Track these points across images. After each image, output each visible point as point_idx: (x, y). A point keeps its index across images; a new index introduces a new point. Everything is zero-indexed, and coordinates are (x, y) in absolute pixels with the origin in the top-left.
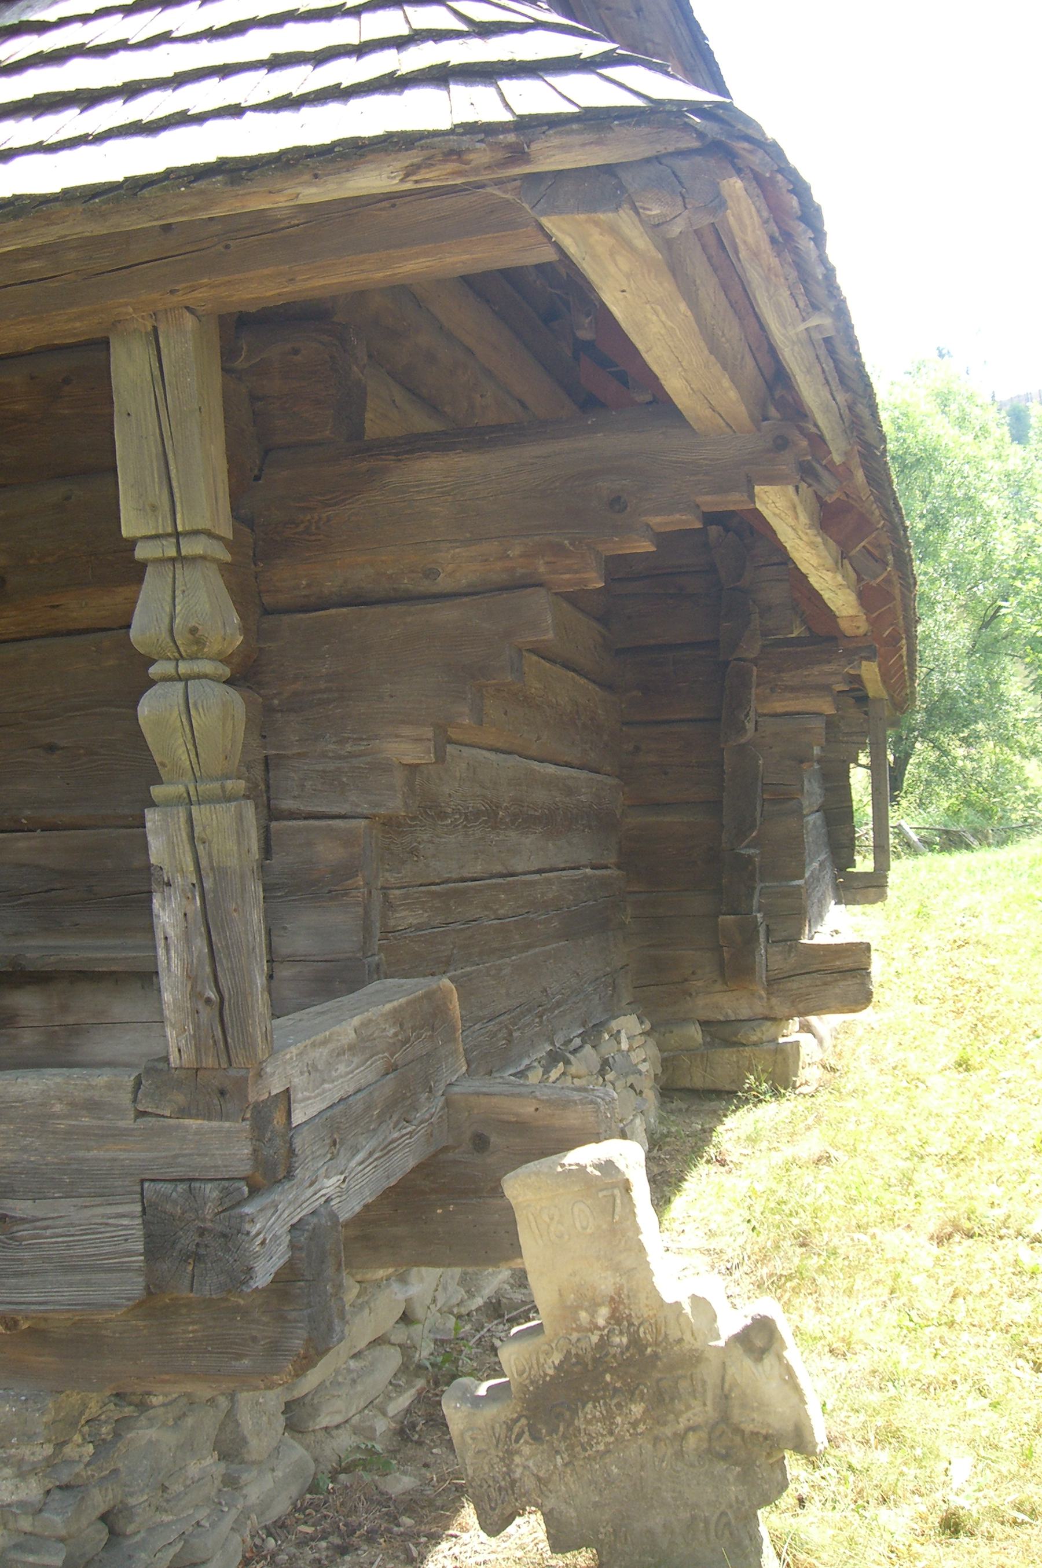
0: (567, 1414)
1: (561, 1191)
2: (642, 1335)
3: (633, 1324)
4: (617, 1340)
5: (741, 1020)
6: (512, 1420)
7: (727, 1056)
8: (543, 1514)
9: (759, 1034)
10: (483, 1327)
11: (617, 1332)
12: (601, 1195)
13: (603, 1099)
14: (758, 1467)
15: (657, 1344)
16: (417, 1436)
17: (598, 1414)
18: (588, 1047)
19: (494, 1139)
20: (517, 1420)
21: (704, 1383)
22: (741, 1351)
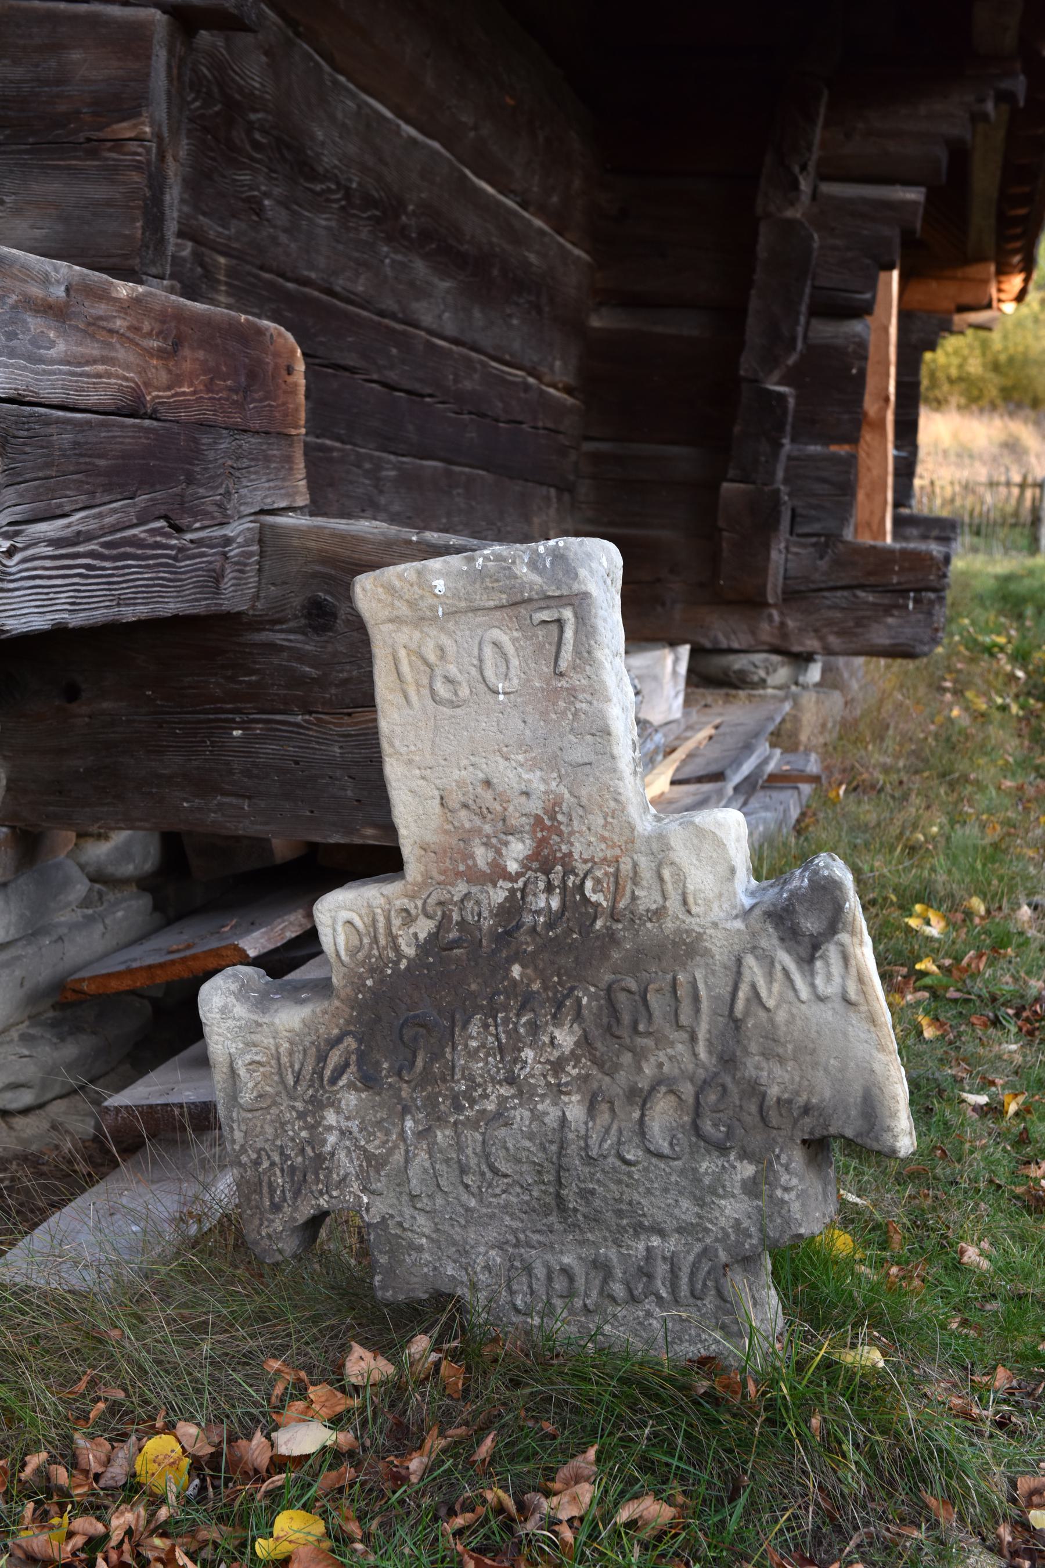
3: (573, 871)
20: (339, 1040)
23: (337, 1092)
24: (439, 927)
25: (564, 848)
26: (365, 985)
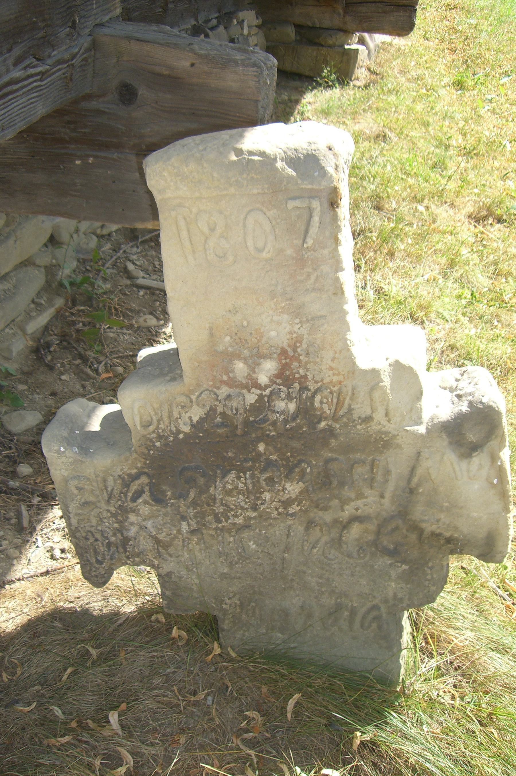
0: (201, 481)
1: (232, 190)
2: (317, 404)
3: (307, 389)
4: (280, 405)
5: (323, 29)
6: (130, 475)
7: (310, 51)
8: (159, 576)
9: (334, 40)
10: (120, 249)
11: (283, 395)
12: (291, 205)
13: (265, 64)
14: (431, 568)
15: (335, 418)
16: (49, 358)
17: (241, 485)
18: (221, 28)
19: (142, 92)
20: (136, 477)
21: (387, 472)
22: (445, 443)
23: (137, 506)
24: (207, 414)
25: (302, 371)
26: (154, 446)
